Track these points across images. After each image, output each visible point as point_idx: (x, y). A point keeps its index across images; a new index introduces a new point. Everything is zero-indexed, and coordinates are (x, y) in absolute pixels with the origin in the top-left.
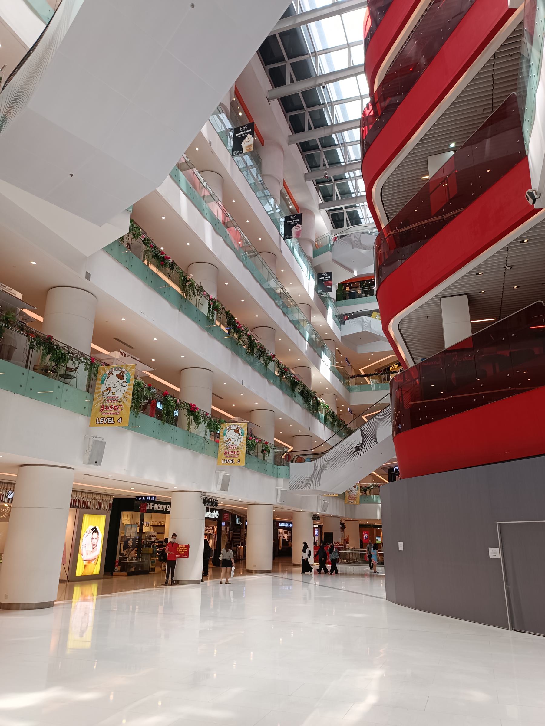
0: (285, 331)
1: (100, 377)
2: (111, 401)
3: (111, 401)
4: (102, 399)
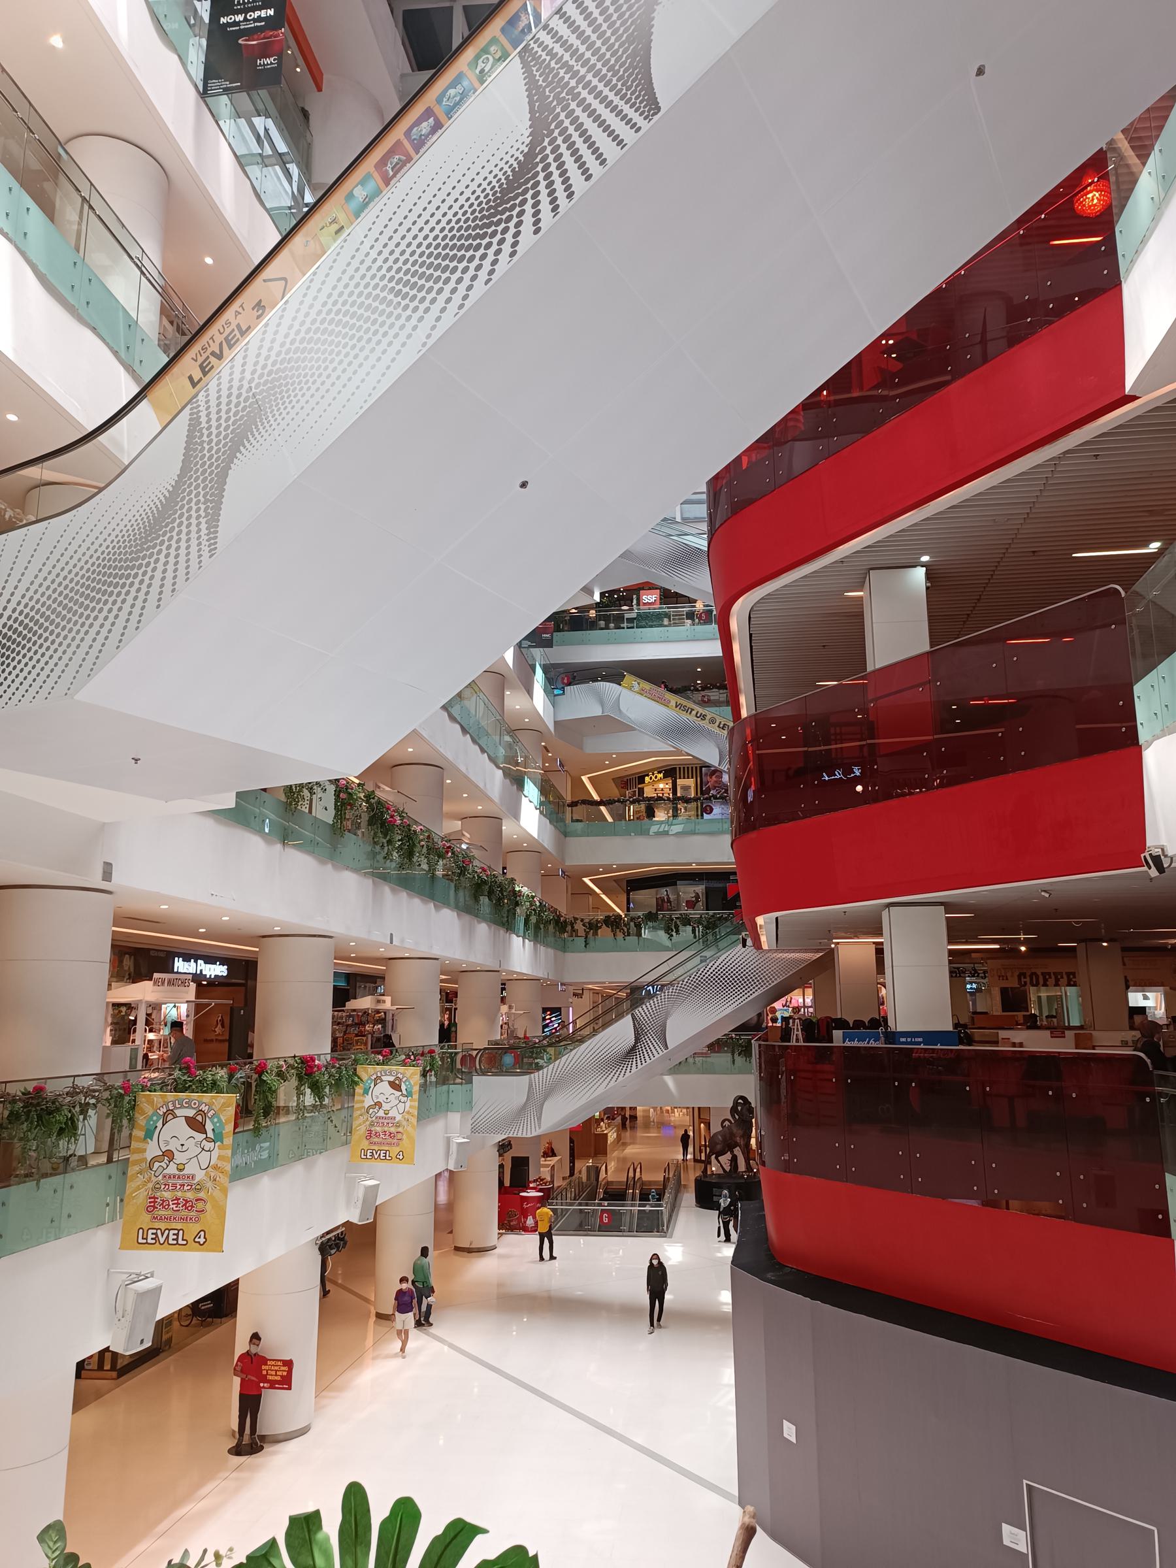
0: (463, 769)
1: (141, 1120)
2: (174, 1185)
3: (174, 1185)
4: (149, 1180)
